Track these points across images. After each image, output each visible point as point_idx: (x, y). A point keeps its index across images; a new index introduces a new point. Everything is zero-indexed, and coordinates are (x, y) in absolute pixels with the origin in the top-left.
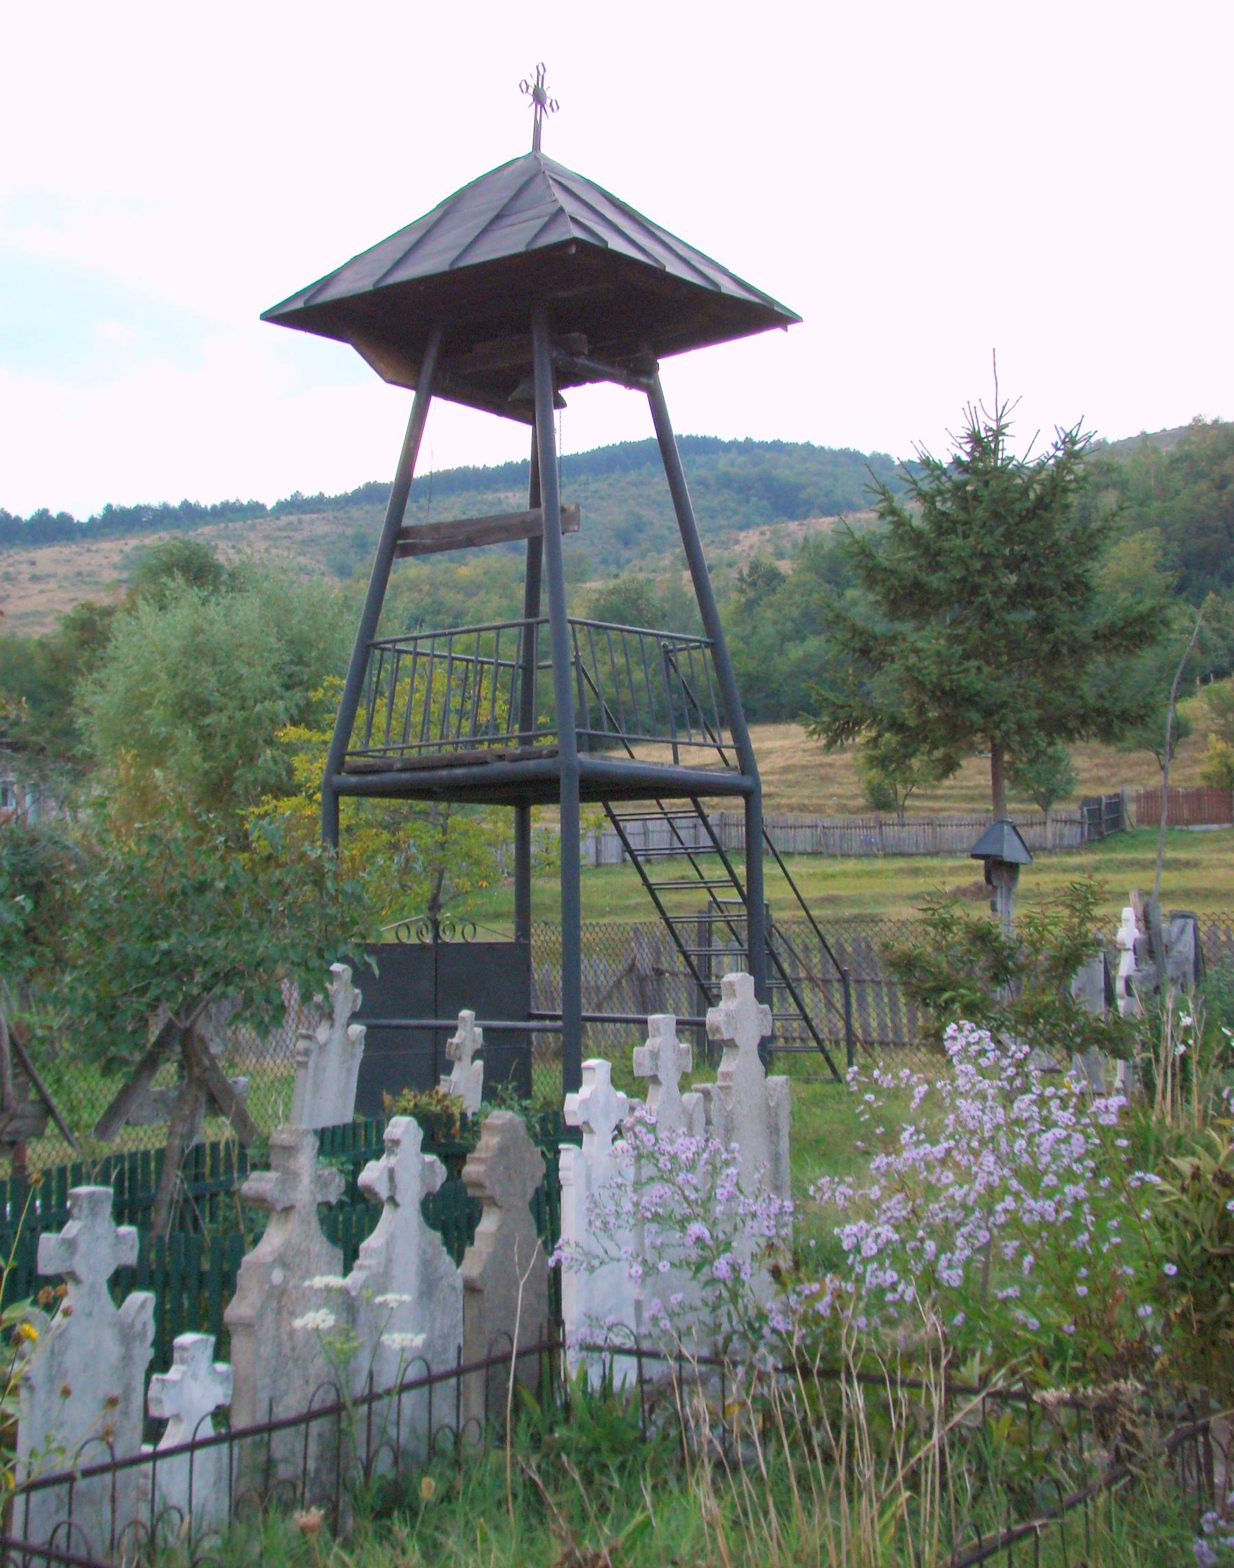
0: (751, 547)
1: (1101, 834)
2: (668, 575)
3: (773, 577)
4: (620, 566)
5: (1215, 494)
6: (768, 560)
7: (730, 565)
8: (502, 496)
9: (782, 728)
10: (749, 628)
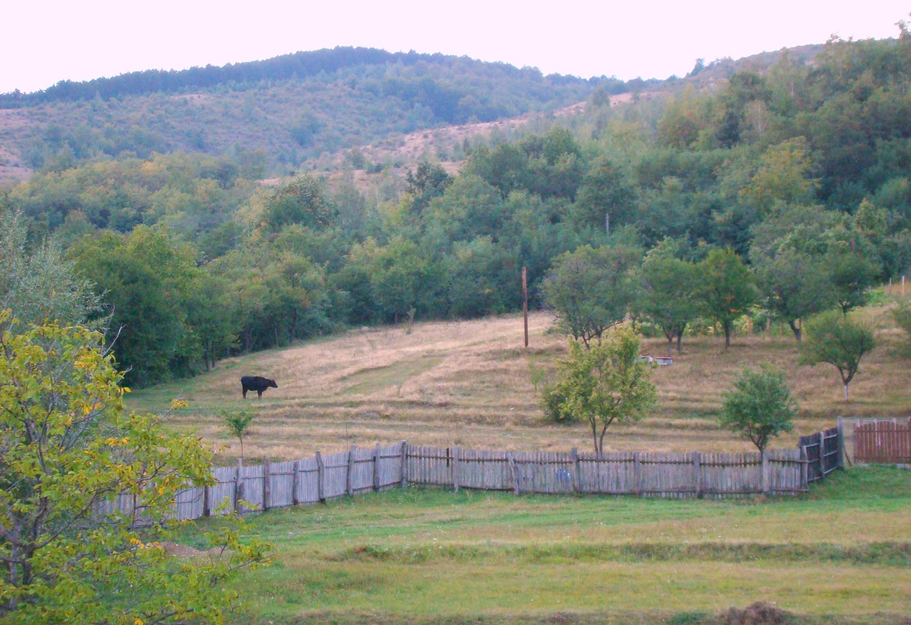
0: (415, 149)
1: (820, 474)
2: (340, 174)
3: (440, 179)
4: (296, 164)
5: (857, 105)
6: (434, 162)
7: (397, 166)
8: (188, 97)
9: (452, 326)
10: (418, 229)
